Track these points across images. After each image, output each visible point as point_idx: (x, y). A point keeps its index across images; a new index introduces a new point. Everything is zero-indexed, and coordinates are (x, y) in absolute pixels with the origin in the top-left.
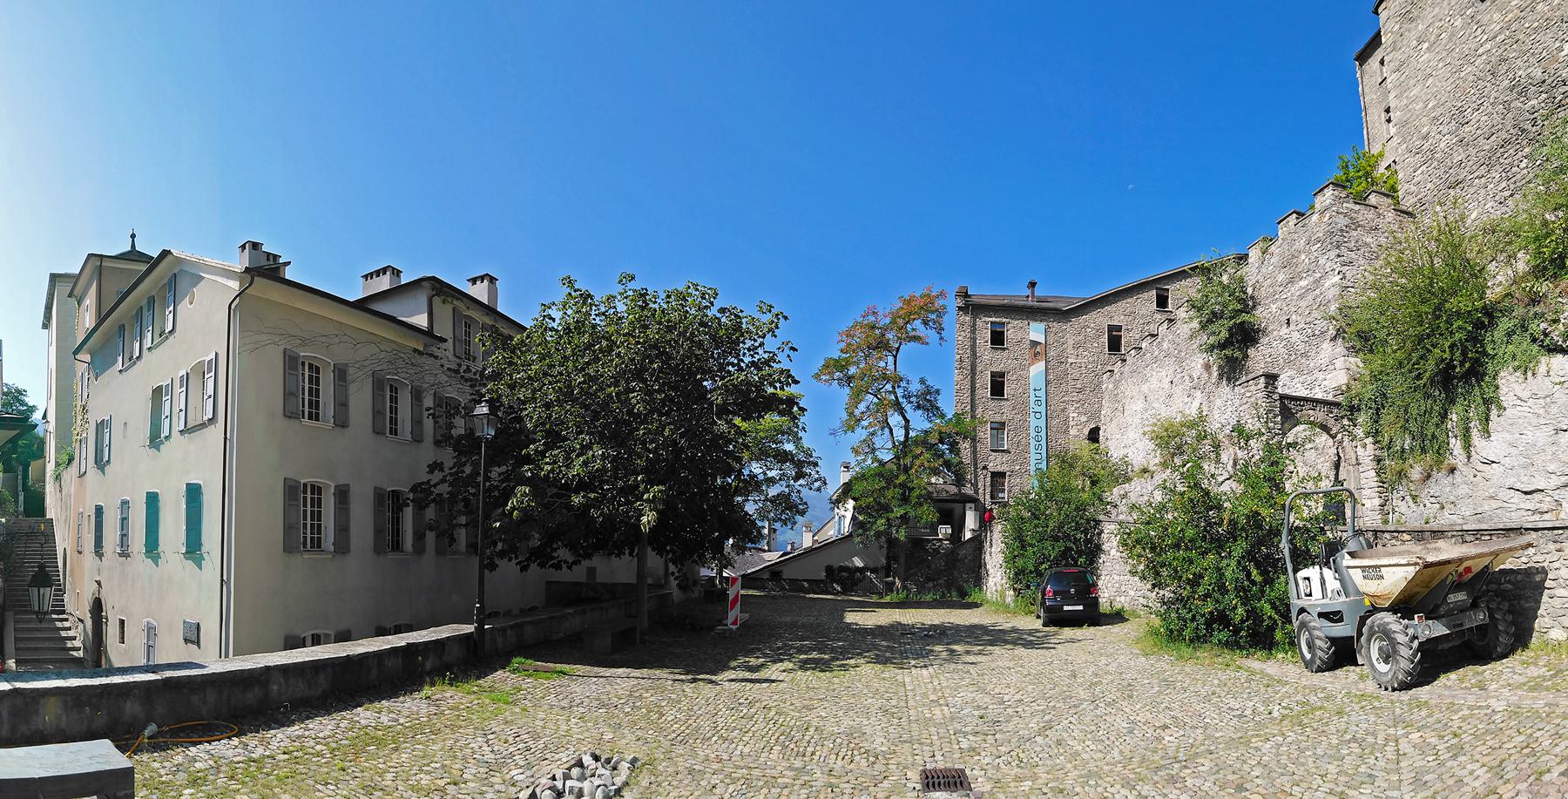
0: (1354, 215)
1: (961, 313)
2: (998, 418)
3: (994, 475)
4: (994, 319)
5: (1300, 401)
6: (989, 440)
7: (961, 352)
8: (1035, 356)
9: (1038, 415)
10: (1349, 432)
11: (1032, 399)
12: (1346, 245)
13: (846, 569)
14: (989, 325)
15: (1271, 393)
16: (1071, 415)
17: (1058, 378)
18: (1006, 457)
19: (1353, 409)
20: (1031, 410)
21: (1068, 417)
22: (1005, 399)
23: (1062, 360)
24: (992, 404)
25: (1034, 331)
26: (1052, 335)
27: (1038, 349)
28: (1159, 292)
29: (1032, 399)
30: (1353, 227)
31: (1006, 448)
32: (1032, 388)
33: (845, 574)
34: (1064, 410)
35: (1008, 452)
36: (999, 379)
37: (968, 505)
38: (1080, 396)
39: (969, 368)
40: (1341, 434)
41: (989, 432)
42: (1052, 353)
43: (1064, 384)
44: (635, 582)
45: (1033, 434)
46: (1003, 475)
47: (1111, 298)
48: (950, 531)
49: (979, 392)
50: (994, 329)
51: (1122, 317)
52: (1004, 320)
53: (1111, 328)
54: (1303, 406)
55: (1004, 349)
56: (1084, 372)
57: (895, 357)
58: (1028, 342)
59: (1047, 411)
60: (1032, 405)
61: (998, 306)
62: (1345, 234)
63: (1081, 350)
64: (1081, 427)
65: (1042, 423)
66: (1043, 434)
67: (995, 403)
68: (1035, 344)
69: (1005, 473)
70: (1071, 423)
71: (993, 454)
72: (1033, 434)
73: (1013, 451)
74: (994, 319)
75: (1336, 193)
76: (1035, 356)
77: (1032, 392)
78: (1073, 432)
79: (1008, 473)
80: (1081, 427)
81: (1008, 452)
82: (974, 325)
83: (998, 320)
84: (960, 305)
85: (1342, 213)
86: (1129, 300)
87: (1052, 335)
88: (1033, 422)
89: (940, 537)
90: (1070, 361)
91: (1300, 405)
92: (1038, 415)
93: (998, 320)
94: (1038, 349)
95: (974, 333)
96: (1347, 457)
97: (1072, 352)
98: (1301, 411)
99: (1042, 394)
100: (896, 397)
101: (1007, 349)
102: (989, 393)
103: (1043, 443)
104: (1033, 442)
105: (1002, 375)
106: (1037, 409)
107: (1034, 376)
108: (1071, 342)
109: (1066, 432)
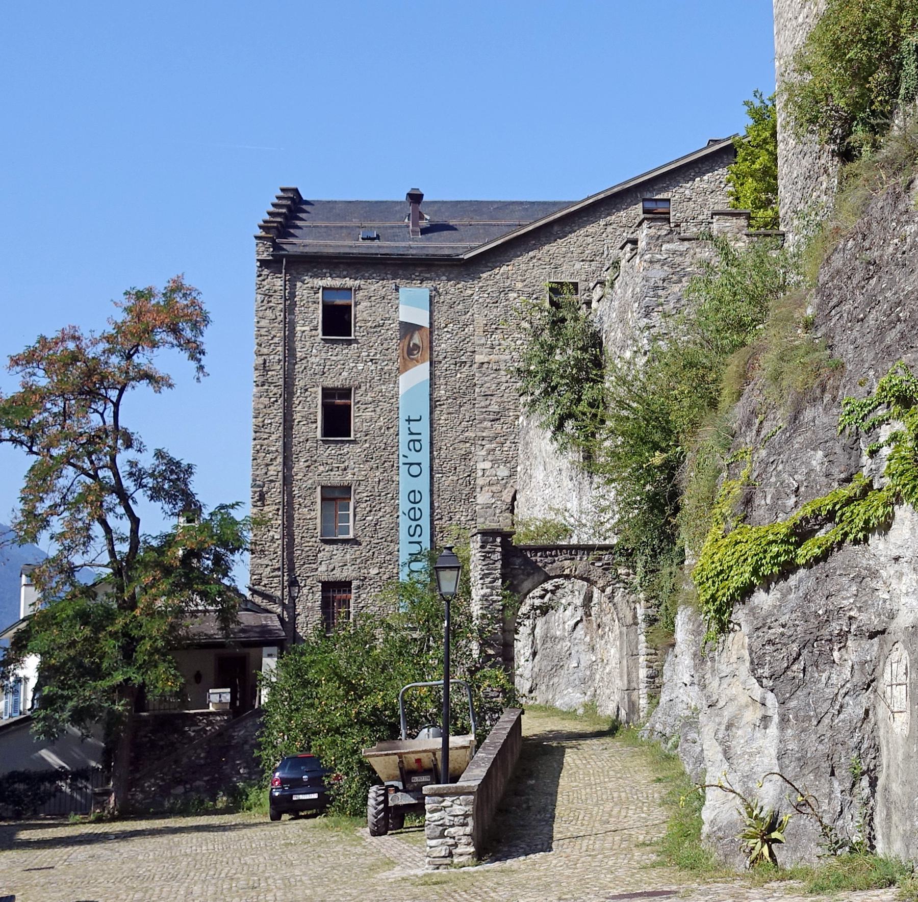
0: (678, 260)
1: (266, 272)
2: (336, 479)
3: (327, 586)
4: (328, 282)
5: (551, 550)
6: (318, 521)
7: (265, 351)
8: (410, 352)
9: (415, 470)
10: (627, 583)
11: (404, 438)
12: (660, 308)
13: (24, 777)
14: (320, 295)
15: (489, 553)
16: (481, 466)
17: (456, 395)
18: (351, 552)
19: (629, 554)
20: (402, 460)
21: (473, 471)
22: (350, 442)
23: (464, 359)
24: (327, 452)
25: (406, 304)
26: (445, 308)
27: (416, 339)
28: (649, 205)
29: (404, 438)
30: (675, 278)
31: (351, 536)
32: (403, 416)
33: (21, 787)
34: (466, 457)
35: (355, 542)
36: (338, 401)
37: (266, 650)
38: (498, 426)
39: (281, 382)
40: (611, 588)
41: (318, 506)
42: (444, 346)
43: (467, 407)
44: (522, 735)
45: (404, 505)
46: (345, 586)
47: (556, 228)
48: (227, 698)
49: (301, 430)
50: (327, 300)
51: (578, 266)
52: (349, 282)
53: (556, 289)
54: (556, 555)
55: (349, 342)
56: (504, 379)
57: (116, 405)
58: (395, 326)
59: (432, 459)
60: (403, 450)
61: (336, 258)
62: (660, 292)
63: (498, 336)
64: (499, 488)
65: (423, 484)
66: (425, 505)
67: (332, 450)
68: (408, 329)
69: (350, 583)
70: (480, 482)
71: (327, 547)
72: (404, 505)
73: (365, 541)
74: (328, 282)
75: (653, 231)
76: (410, 352)
77: (403, 426)
78: (482, 498)
79: (355, 584)
80: (499, 488)
81: (355, 542)
82: (293, 295)
83: (337, 283)
84: (264, 256)
85: (659, 261)
86: (591, 229)
87: (445, 308)
88: (405, 483)
89: (212, 709)
90: (479, 358)
91: (551, 556)
92: (415, 470)
93: (337, 283)
94: (416, 339)
95: (292, 312)
96: (621, 615)
97: (483, 341)
98: (551, 563)
99: (423, 427)
100: (116, 474)
101: (356, 341)
102: (319, 429)
103: (425, 522)
104: (404, 523)
105: (346, 393)
106: (413, 457)
107: (408, 392)
108: (480, 320)
109: (470, 498)
